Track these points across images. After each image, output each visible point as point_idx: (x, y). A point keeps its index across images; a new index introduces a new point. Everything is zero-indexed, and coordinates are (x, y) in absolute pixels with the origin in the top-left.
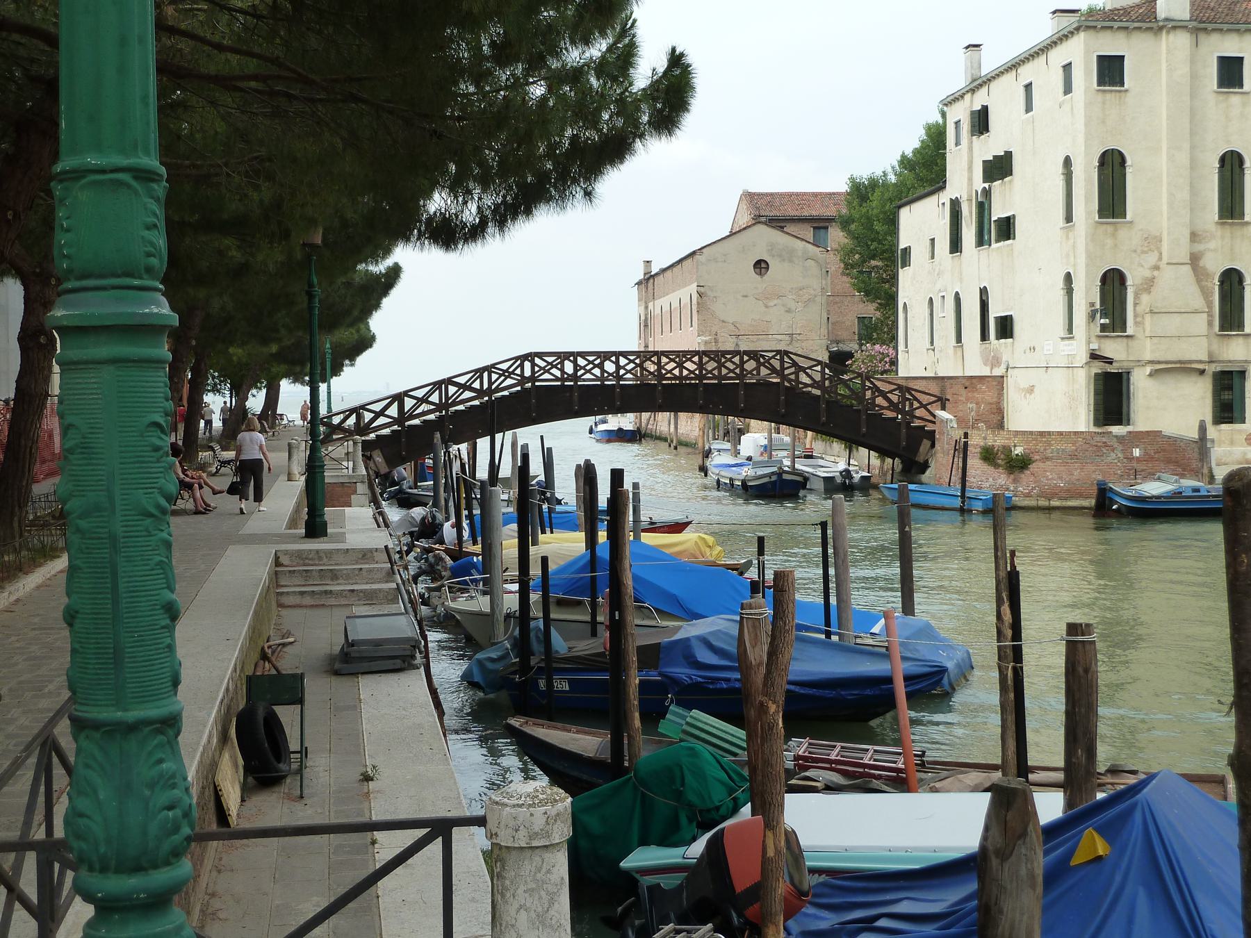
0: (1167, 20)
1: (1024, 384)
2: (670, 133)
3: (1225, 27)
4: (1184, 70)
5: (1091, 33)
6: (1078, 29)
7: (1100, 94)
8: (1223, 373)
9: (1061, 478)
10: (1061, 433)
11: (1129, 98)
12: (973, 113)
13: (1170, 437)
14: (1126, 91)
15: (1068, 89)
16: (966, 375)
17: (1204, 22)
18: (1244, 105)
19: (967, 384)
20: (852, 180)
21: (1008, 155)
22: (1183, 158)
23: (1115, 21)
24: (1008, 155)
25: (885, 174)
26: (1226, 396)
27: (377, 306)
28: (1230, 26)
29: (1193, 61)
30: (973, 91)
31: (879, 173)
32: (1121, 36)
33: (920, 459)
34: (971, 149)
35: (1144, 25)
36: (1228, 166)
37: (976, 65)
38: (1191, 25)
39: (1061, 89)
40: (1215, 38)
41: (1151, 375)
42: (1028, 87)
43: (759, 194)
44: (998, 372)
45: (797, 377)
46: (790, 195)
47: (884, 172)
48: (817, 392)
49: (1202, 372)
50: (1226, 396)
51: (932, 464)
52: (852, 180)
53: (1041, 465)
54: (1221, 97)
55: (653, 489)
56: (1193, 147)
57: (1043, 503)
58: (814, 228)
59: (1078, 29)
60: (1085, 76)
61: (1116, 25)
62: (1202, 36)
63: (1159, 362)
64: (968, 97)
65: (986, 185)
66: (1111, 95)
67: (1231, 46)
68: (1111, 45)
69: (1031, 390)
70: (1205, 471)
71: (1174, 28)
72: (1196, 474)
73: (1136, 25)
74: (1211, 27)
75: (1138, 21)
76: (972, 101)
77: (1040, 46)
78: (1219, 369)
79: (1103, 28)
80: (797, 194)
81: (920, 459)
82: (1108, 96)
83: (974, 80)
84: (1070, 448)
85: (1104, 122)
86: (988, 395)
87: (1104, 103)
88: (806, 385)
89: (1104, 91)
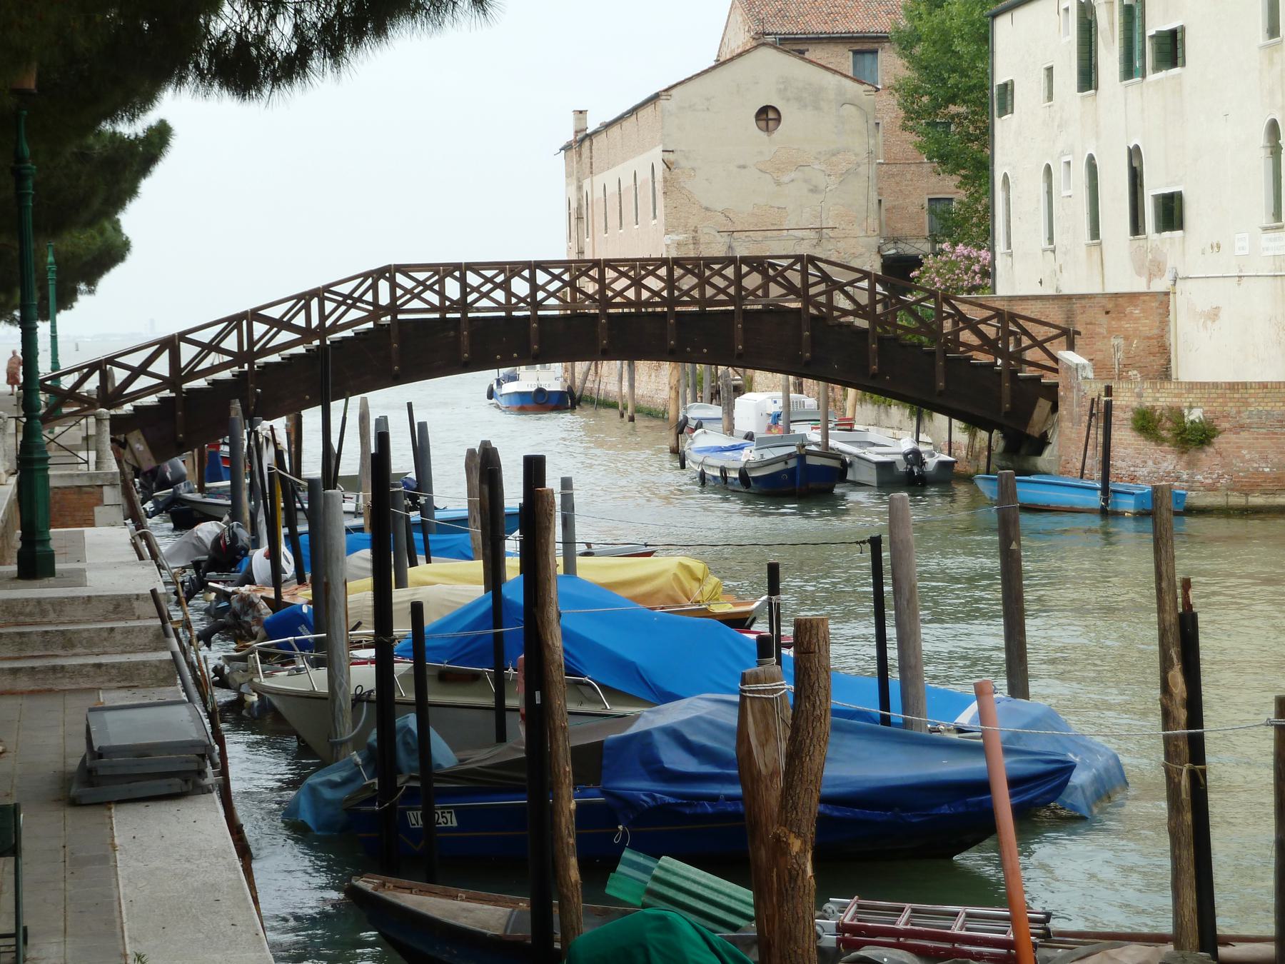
9: (1265, 459)
10: (1264, 385)
19: (1110, 306)
44: (1160, 285)
45: (830, 299)
51: (1054, 439)
57: (1236, 500)
69: (1214, 314)
81: (1034, 430)
86: (1147, 326)
88: (845, 313)
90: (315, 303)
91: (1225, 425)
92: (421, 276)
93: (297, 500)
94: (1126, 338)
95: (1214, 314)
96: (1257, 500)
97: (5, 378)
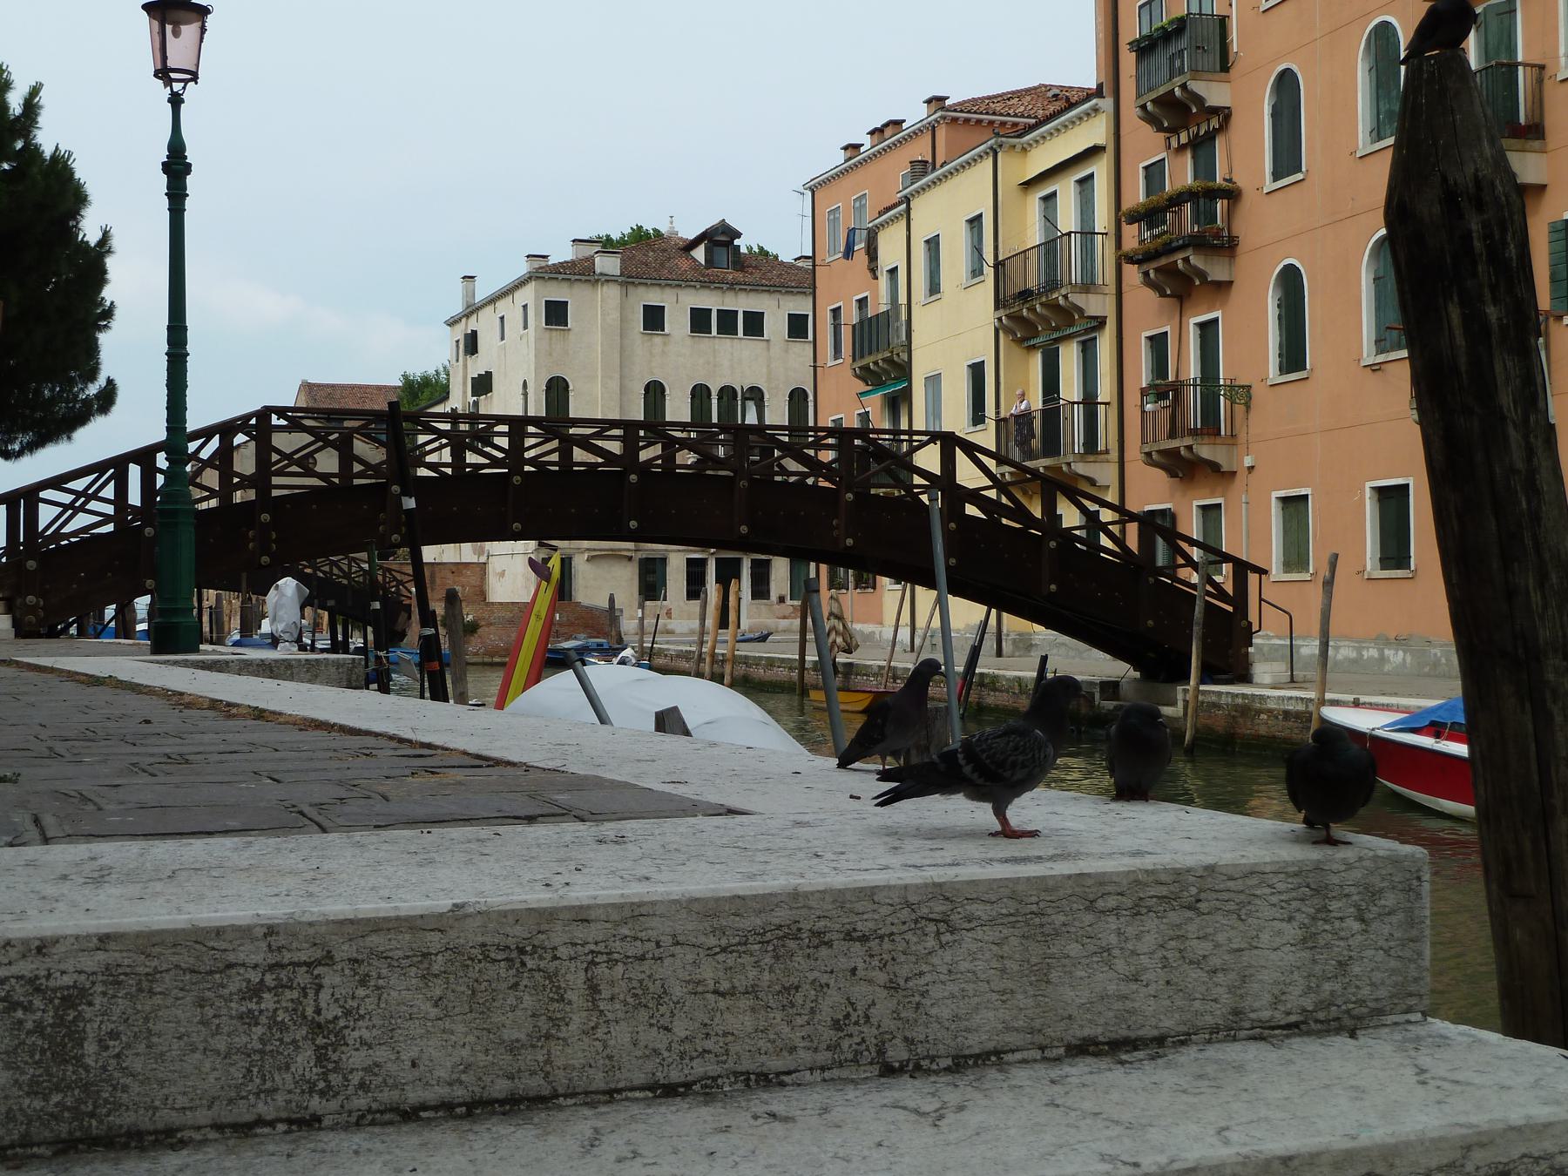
0: (601, 274)
1: (499, 570)
2: (106, 414)
3: (649, 282)
4: (616, 315)
5: (540, 282)
6: (530, 278)
7: (548, 332)
8: (647, 559)
9: (501, 639)
10: (501, 604)
11: (572, 336)
12: (466, 335)
13: (587, 607)
14: (569, 330)
15: (525, 327)
16: (463, 561)
17: (633, 277)
18: (665, 344)
19: (454, 569)
20: (405, 376)
21: (489, 375)
22: (614, 385)
23: (561, 273)
24: (489, 375)
25: (437, 373)
26: (650, 578)
27: (1420, 423)
28: (654, 282)
29: (622, 308)
30: (467, 316)
31: (431, 372)
32: (565, 285)
33: (399, 628)
34: (465, 366)
35: (583, 278)
36: (651, 392)
37: (470, 294)
38: (620, 279)
39: (522, 325)
40: (641, 290)
41: (588, 560)
42: (502, 318)
43: (319, 386)
44: (483, 559)
45: (331, 569)
46: (353, 387)
47: (436, 371)
48: (345, 582)
49: (630, 558)
50: (650, 578)
51: (409, 633)
52: (405, 376)
53: (487, 629)
54: (646, 338)
55: (426, 984)
56: (621, 377)
57: (487, 660)
58: (854, 326)
59: (530, 278)
60: (537, 317)
61: (560, 277)
62: (631, 288)
63: (595, 550)
64: (464, 320)
65: (475, 398)
66: (556, 333)
67: (654, 297)
68: (558, 293)
69: (502, 574)
70: (613, 633)
71: (607, 281)
72: (606, 635)
73: (577, 277)
74: (637, 281)
75: (580, 274)
76: (467, 324)
77: (508, 288)
78: (644, 556)
79: (549, 278)
80: (360, 387)
81: (399, 628)
82: (554, 333)
83: (468, 307)
84: (509, 615)
85: (550, 355)
86: (474, 580)
87: (551, 339)
88: (339, 577)
89: (551, 329)
90: (134, 471)
91: (483, 623)
92: (79, 485)
93: (160, 480)
94: (463, 586)
95: (502, 574)
96: (497, 660)
97: (648, 226)
